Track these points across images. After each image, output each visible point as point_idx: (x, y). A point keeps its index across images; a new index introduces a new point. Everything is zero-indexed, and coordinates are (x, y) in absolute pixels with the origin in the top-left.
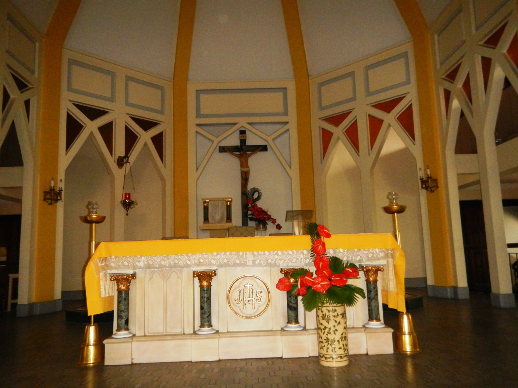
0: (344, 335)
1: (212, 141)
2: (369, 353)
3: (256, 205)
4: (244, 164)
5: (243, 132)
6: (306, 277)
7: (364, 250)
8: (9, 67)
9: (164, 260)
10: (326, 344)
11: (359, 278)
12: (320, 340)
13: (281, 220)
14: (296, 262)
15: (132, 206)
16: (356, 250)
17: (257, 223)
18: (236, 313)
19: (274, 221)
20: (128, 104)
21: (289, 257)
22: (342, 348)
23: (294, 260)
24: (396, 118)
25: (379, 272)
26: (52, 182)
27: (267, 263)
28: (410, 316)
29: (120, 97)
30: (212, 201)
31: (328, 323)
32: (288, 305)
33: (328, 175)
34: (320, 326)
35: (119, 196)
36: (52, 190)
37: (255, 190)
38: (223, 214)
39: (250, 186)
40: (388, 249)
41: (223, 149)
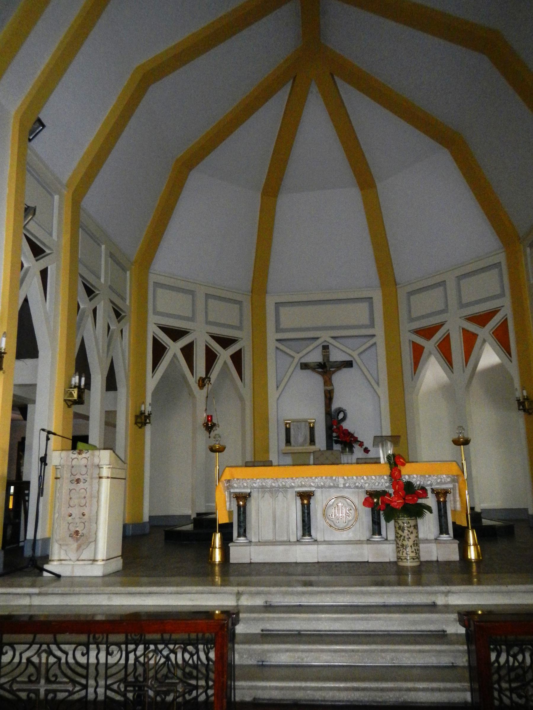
0: (416, 542)
1: (293, 357)
2: (439, 560)
3: (342, 427)
4: (328, 382)
5: (325, 348)
6: (386, 497)
7: (434, 476)
8: (112, 302)
9: (274, 483)
10: (402, 549)
11: (428, 498)
12: (398, 546)
13: (368, 443)
14: (378, 485)
15: (214, 429)
16: (427, 476)
17: (343, 446)
18: (331, 526)
19: (361, 444)
20: (208, 323)
21: (373, 481)
22: (414, 551)
23: (377, 484)
24: (491, 333)
25: (448, 494)
26: (143, 406)
27: (355, 486)
28: (474, 531)
29: (200, 317)
30: (294, 422)
31: (403, 532)
32: (373, 520)
33: (421, 391)
34: (397, 535)
35: (202, 417)
36: (142, 413)
37: (340, 410)
38: (306, 436)
39: (335, 406)
40: (454, 476)
41: (305, 366)
